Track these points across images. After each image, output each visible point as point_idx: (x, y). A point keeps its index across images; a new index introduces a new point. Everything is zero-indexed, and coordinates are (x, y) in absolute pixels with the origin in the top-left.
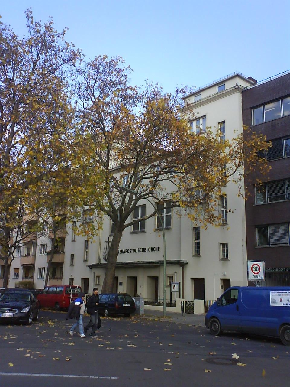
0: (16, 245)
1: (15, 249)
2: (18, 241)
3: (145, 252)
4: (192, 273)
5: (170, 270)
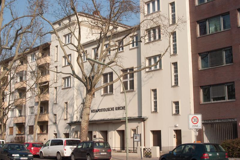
0: (9, 108)
1: (8, 111)
2: (11, 104)
3: (113, 110)
4: (152, 125)
5: (134, 125)
